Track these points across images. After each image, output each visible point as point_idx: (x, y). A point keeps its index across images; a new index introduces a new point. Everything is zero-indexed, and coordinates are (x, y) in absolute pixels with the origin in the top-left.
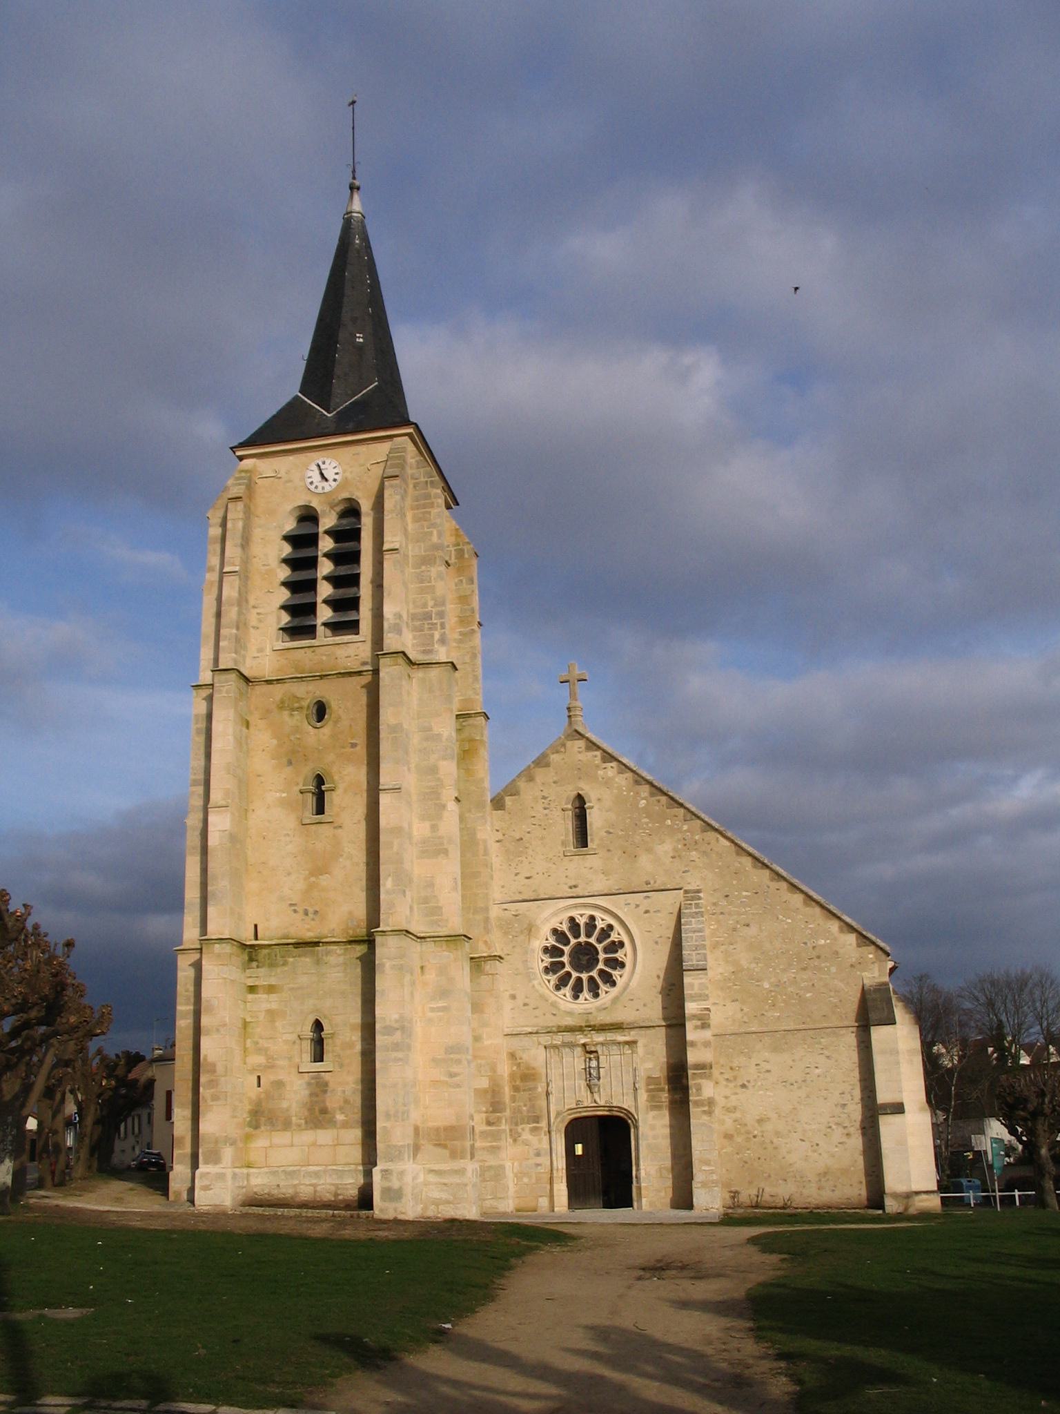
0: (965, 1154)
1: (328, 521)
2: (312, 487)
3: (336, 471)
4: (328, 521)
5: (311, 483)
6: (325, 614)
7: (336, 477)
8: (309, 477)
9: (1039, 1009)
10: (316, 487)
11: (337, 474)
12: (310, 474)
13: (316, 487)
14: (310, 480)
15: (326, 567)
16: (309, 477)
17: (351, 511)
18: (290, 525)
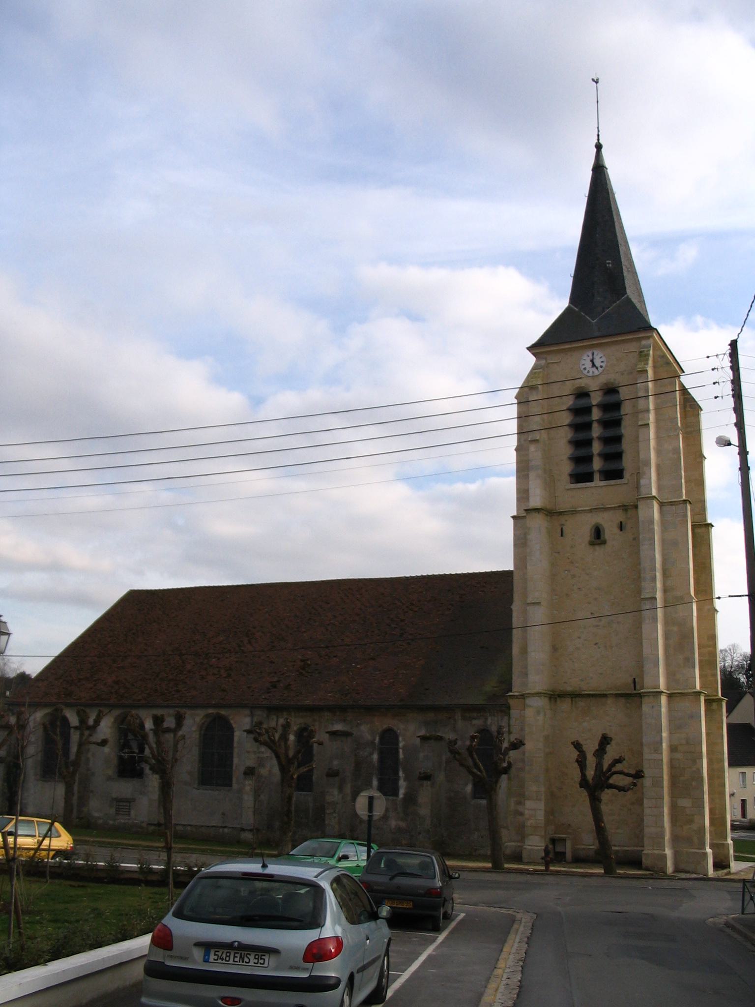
0: (366, 843)
1: (596, 399)
2: (585, 372)
3: (602, 360)
4: (596, 399)
5: (585, 369)
6: (597, 464)
7: (602, 364)
8: (583, 365)
9: (106, 911)
10: (588, 372)
11: (602, 362)
12: (583, 362)
13: (588, 372)
14: (584, 367)
15: (596, 431)
16: (583, 365)
17: (611, 390)
18: (570, 402)
